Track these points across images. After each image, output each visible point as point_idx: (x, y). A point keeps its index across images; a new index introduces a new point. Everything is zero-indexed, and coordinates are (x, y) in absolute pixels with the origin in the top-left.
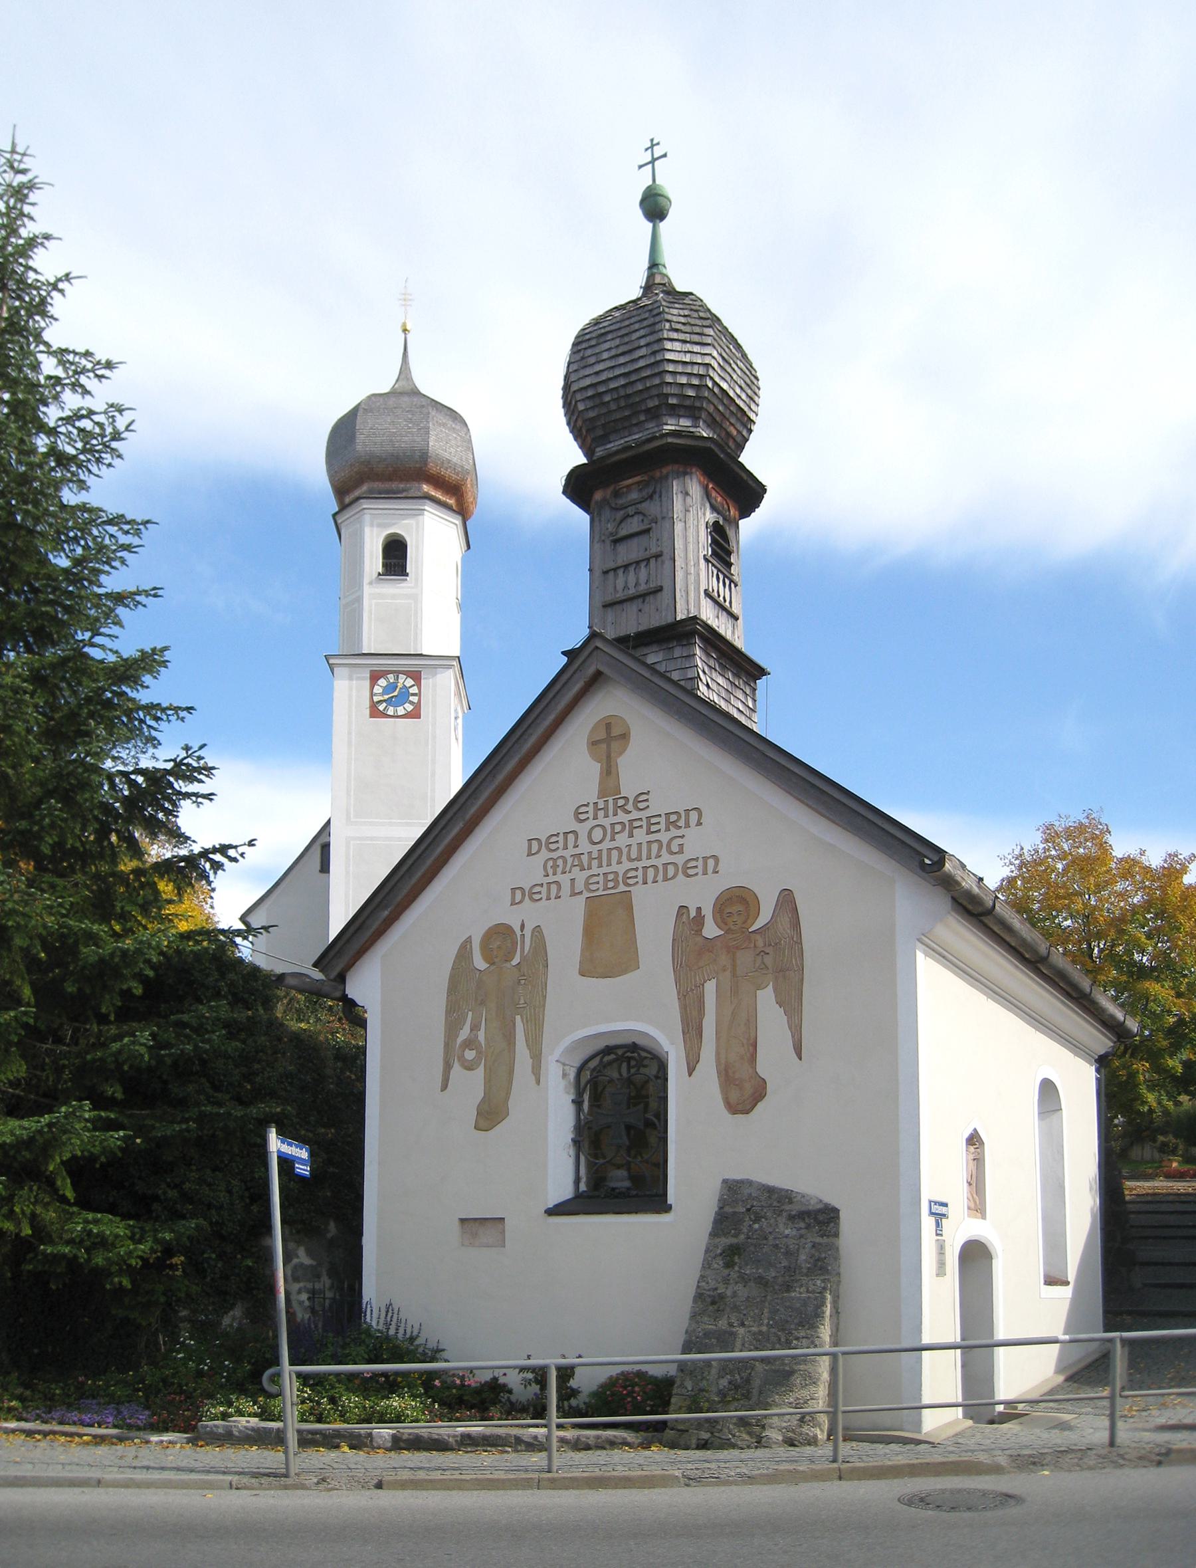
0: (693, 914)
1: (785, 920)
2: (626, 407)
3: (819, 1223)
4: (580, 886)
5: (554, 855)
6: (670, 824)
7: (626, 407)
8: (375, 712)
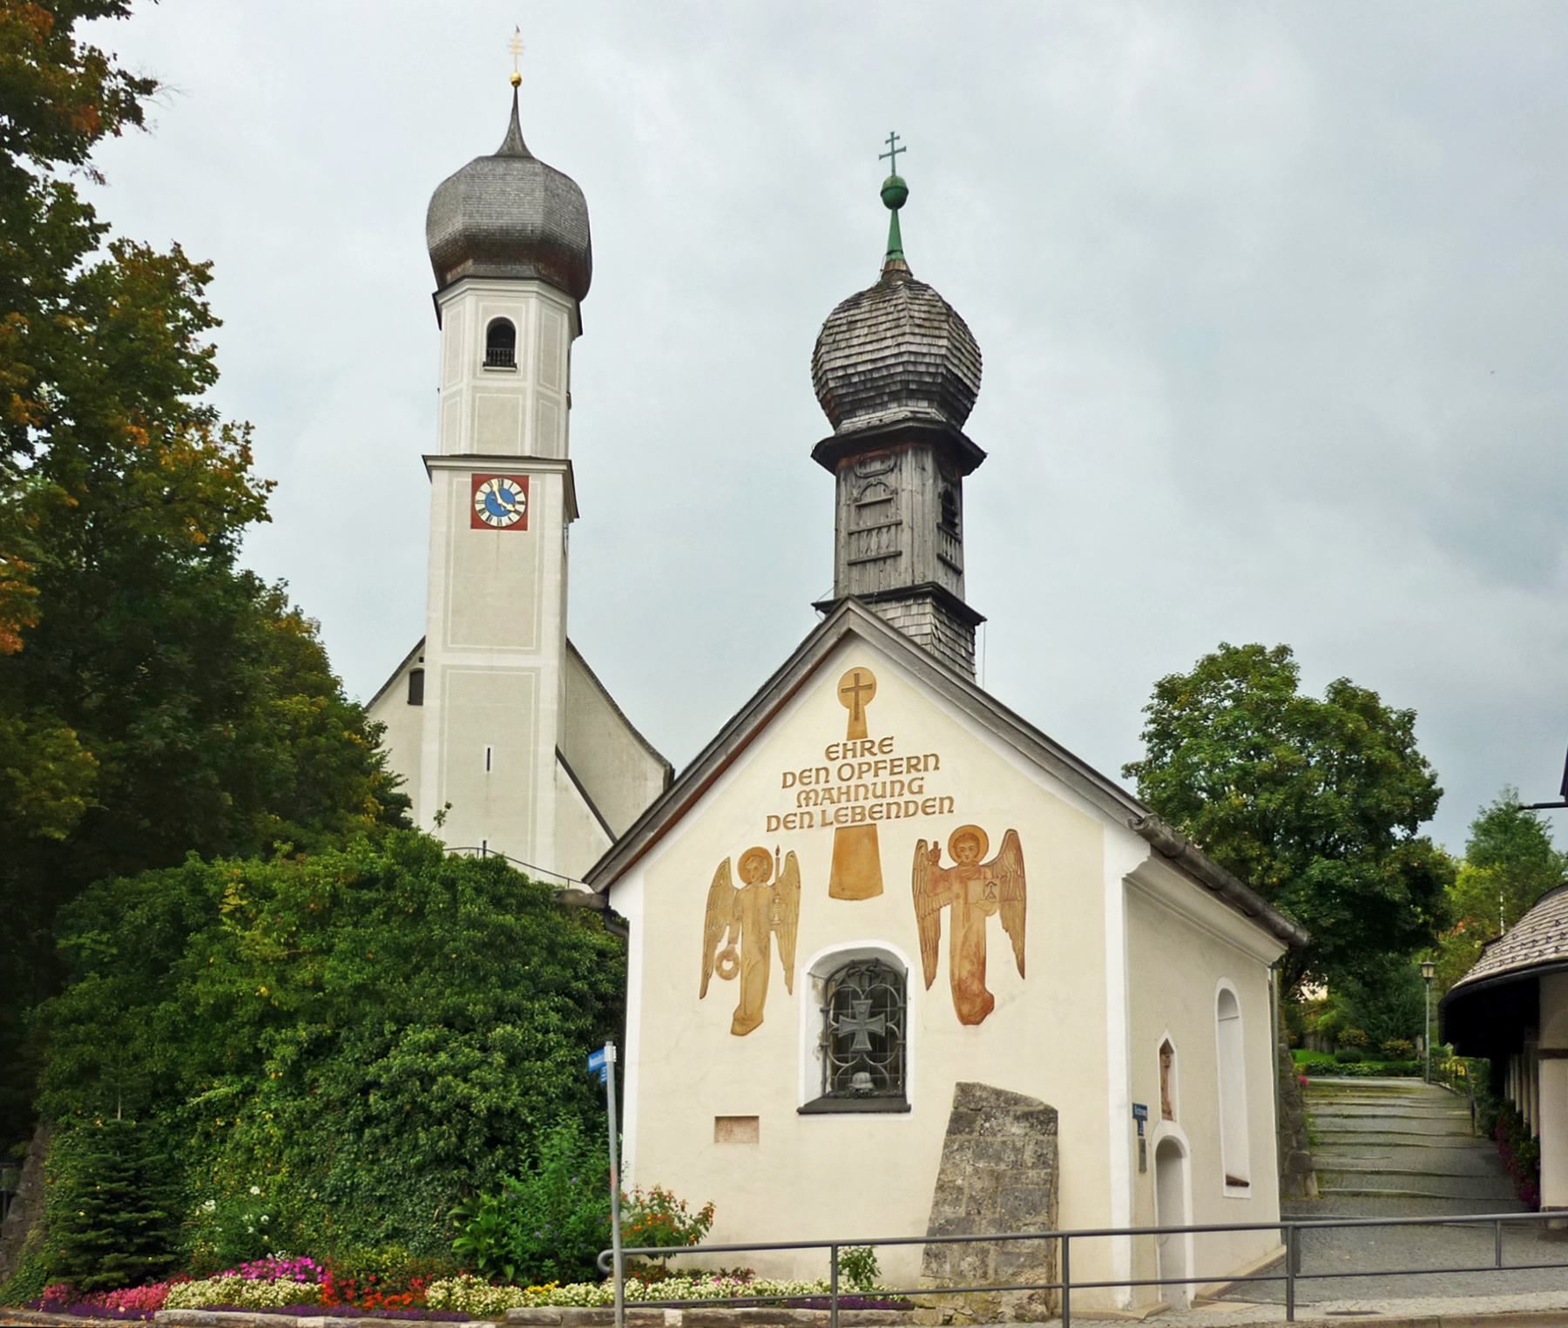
0: (931, 847)
1: (1010, 857)
2: (872, 388)
3: (1041, 1123)
4: (830, 817)
5: (807, 788)
6: (910, 767)
7: (872, 388)
8: (477, 523)
